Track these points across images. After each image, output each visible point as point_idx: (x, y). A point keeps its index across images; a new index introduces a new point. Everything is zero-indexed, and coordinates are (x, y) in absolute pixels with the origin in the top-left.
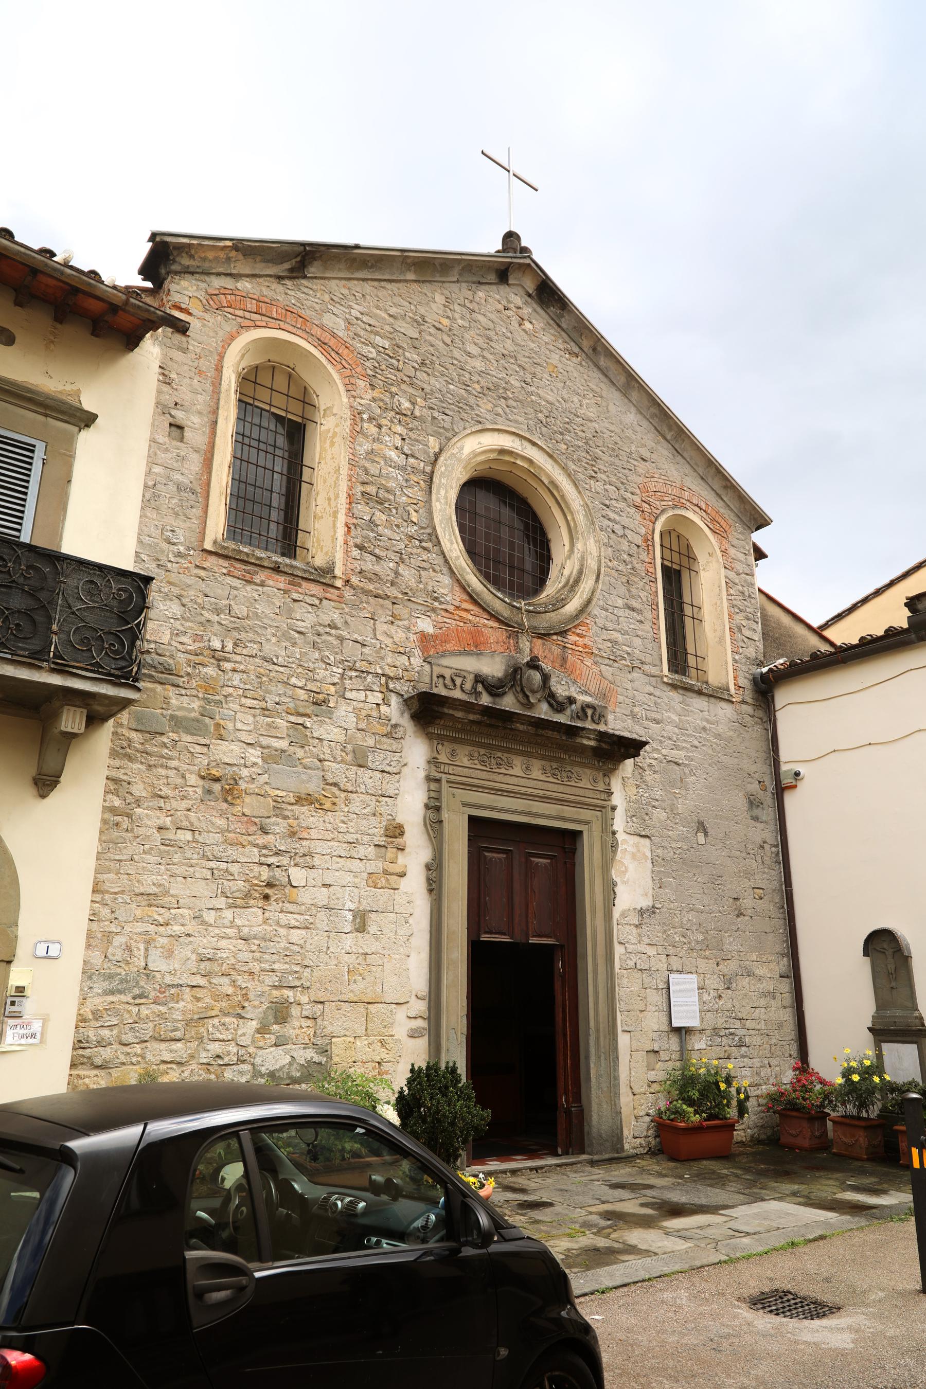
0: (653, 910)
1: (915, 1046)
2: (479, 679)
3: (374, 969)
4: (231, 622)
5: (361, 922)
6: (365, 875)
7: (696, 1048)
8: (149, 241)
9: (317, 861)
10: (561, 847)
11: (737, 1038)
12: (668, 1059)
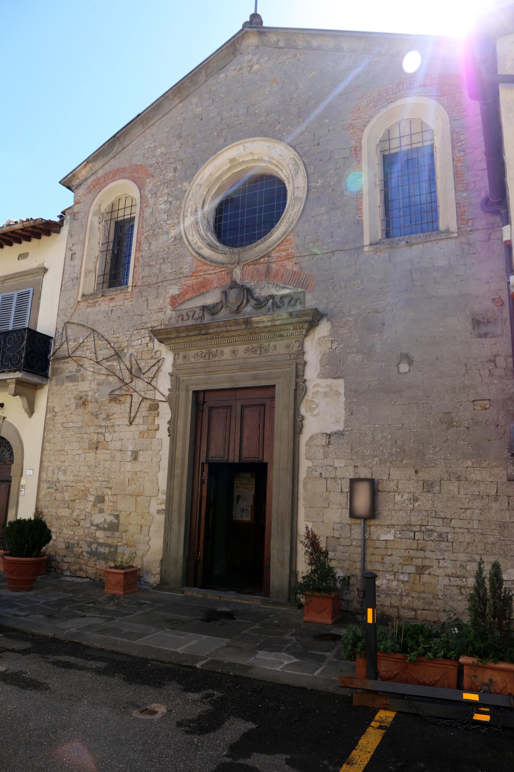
0: (340, 434)
1: (499, 73)
2: (204, 308)
3: (140, 479)
4: (246, 272)
5: (135, 456)
6: (138, 433)
7: (382, 539)
8: (68, 183)
9: (117, 428)
10: (258, 401)
11: (435, 534)
12: (349, 544)
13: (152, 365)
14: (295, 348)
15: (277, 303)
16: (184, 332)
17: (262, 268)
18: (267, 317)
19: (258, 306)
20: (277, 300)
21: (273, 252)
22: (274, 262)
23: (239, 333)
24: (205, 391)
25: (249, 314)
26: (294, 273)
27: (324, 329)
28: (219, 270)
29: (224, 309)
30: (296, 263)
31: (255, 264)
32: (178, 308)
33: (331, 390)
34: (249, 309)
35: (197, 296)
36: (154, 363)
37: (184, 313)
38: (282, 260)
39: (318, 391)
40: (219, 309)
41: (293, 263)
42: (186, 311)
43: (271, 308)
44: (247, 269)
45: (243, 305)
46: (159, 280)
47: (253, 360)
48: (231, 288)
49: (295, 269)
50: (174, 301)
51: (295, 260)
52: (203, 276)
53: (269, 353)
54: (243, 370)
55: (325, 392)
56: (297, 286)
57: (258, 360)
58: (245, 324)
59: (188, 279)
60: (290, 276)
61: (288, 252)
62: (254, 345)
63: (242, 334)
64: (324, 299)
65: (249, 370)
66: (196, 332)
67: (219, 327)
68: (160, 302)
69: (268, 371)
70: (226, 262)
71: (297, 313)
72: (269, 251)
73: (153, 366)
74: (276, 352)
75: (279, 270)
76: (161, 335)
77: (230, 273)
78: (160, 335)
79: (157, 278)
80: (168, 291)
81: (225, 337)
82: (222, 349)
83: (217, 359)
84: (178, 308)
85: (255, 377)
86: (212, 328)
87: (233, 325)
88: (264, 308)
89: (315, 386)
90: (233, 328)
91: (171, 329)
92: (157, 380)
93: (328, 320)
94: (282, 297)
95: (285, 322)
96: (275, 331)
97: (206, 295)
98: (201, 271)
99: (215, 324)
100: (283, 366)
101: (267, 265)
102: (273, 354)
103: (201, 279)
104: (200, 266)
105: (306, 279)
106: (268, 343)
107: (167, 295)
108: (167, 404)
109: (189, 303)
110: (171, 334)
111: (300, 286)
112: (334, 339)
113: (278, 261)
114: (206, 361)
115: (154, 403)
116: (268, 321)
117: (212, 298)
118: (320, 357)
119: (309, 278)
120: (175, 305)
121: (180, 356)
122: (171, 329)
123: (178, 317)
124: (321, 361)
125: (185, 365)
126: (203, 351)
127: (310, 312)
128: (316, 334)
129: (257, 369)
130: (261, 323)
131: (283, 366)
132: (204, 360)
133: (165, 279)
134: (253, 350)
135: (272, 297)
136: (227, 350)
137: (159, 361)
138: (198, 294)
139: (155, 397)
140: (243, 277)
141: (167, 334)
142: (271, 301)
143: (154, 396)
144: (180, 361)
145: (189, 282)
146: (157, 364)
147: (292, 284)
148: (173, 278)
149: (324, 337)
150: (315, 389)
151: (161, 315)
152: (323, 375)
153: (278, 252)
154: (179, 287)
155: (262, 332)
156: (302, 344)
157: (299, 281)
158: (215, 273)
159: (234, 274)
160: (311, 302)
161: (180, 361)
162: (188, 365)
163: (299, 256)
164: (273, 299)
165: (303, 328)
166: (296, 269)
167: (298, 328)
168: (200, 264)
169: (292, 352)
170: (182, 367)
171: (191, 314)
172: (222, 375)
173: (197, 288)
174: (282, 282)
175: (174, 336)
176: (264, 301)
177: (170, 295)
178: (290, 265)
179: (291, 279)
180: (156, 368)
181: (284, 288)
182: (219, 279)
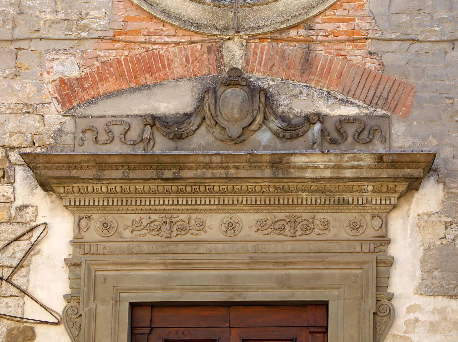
2: (154, 121)
4: (255, 53)
13: (13, 237)
14: (370, 231)
15: (335, 134)
16: (117, 169)
17: (293, 50)
18: (326, 158)
19: (288, 134)
20: (330, 126)
21: (317, 20)
22: (321, 42)
23: (251, 186)
24: (153, 306)
25: (265, 148)
26: (366, 74)
27: (430, 197)
28: (187, 38)
29: (203, 128)
30: (370, 53)
31: (277, 40)
32: (80, 111)
33: (445, 319)
34: (264, 137)
35: (133, 90)
36: (18, 234)
37: (100, 125)
38: (339, 42)
39: (417, 320)
40: (194, 128)
41: (364, 52)
42: (103, 122)
43: (319, 141)
44: (256, 47)
45: (253, 127)
46: (18, 34)
47: (279, 247)
48: (228, 84)
49: (368, 65)
50: (68, 93)
51: (370, 45)
52: (146, 46)
53: (313, 236)
54: (256, 266)
55: (431, 323)
56: (374, 102)
57: (288, 247)
58: (272, 167)
59: (103, 45)
60: (357, 79)
61: (353, 25)
62: (280, 216)
63: (258, 189)
64: (431, 138)
65: (271, 266)
66: (149, 173)
67: (210, 168)
68: (26, 90)
69: (312, 272)
70: (204, 22)
71: (395, 158)
72: (311, 15)
73: (16, 239)
74: (330, 235)
75: (331, 62)
76: (52, 171)
77: (216, 50)
78: (50, 169)
79: (13, 28)
80: (48, 65)
81: (214, 192)
82: (200, 216)
83: (189, 237)
84: (80, 111)
85: (283, 283)
86: (191, 168)
87: (244, 168)
88: (301, 139)
89: (410, 310)
90: (243, 174)
91: (84, 158)
92: (27, 275)
93: (438, 182)
94: (343, 121)
95: (365, 175)
96: (333, 192)
97: (157, 91)
98: (138, 32)
99: (202, 159)
100: (348, 263)
101: (304, 45)
102: (321, 238)
103: (138, 51)
104: (136, 20)
105: (393, 92)
106: (312, 215)
107: (46, 76)
108: (61, 328)
109: (110, 102)
110: (81, 168)
111: (380, 103)
112: (450, 219)
113: (330, 42)
114: (163, 239)
115: (22, 325)
116: (326, 168)
117: (173, 101)
118: (421, 253)
119: (400, 89)
120: (70, 102)
121: (93, 223)
122: (84, 158)
123: (84, 132)
124: (423, 261)
125: (107, 245)
126: (154, 217)
127: (422, 159)
128: (413, 206)
129: (287, 266)
130: (310, 171)
131: (348, 263)
132: (158, 238)
133: (37, 35)
134: (277, 225)
135: (320, 117)
136: (214, 223)
137: (31, 230)
138: (133, 85)
139: (23, 313)
140: (247, 64)
141: (69, 168)
142: (317, 127)
143: (20, 310)
144: (93, 234)
145: (109, 53)
146: (25, 237)
147: (363, 97)
148: (59, 34)
149: (430, 215)
150: (412, 316)
151: (31, 122)
152: (428, 289)
153: (330, 20)
154: (82, 62)
155: (303, 191)
156: (385, 225)
157: (378, 94)
158: (177, 44)
159: (225, 54)
160: (402, 137)
161: (93, 234)
162: (115, 245)
163: (378, 39)
164: (322, 123)
165: (395, 191)
166: (370, 65)
167: (384, 189)
168: (133, 13)
169: (363, 237)
170: (101, 247)
171: (117, 130)
172: (205, 272)
173: (129, 71)
174: (340, 89)
175: (89, 174)
176: (302, 125)
177: (53, 76)
178: (357, 55)
179: (361, 86)
180: (24, 245)
181: (345, 102)
182: (187, 60)
